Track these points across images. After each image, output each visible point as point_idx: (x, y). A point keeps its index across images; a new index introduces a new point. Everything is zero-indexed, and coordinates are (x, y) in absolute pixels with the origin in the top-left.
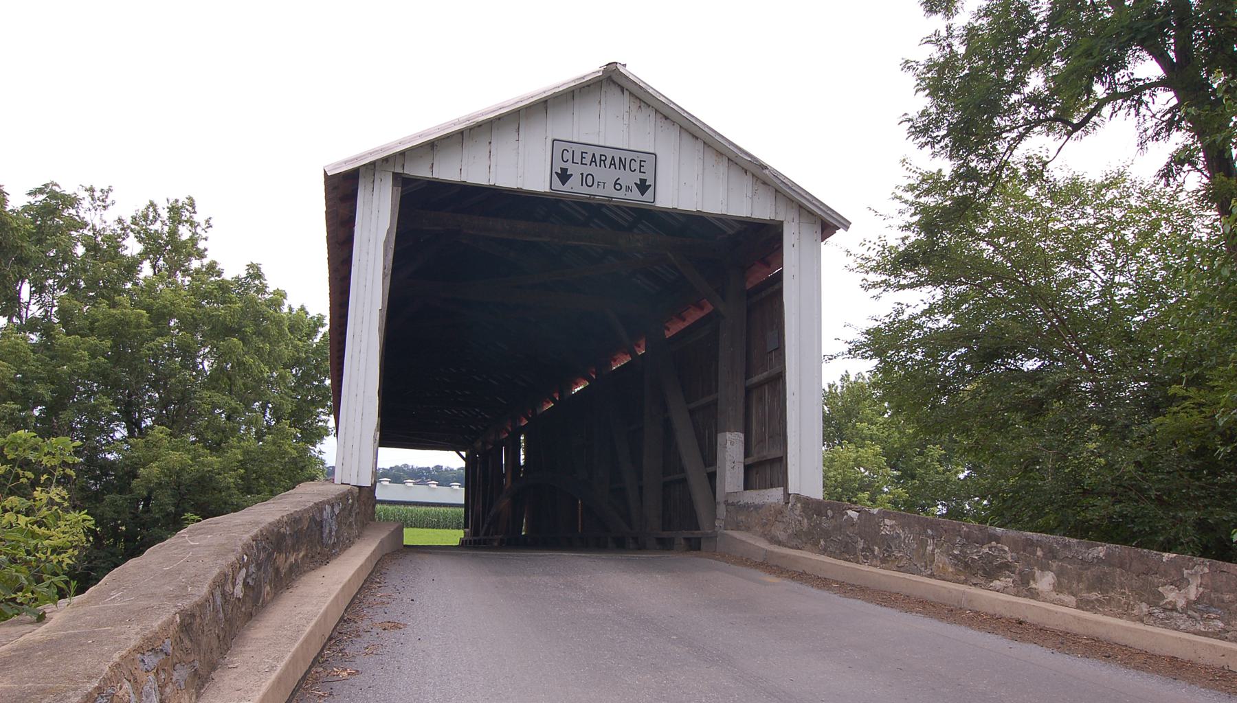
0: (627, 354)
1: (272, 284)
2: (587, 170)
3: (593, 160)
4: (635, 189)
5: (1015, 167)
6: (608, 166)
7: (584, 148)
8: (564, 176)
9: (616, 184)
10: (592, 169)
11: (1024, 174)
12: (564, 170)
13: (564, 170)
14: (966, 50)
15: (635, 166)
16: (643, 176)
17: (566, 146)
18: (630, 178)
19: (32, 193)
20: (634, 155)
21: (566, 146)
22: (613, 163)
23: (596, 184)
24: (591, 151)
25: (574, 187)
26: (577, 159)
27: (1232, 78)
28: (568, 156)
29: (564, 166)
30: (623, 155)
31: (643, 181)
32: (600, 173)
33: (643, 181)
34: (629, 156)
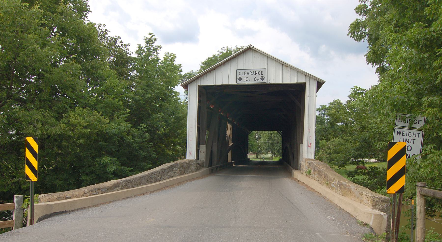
0: (255, 154)
1: (354, 17)
2: (246, 76)
3: (248, 73)
4: (260, 79)
5: (375, 119)
6: (252, 74)
7: (245, 71)
8: (240, 79)
9: (255, 79)
10: (248, 76)
11: (417, 167)
12: (240, 78)
13: (240, 78)
14: (374, 89)
15: (260, 73)
16: (262, 76)
17: (240, 71)
18: (258, 77)
19: (349, 30)
20: (259, 70)
21: (240, 71)
22: (253, 73)
23: (249, 80)
24: (247, 71)
25: (243, 82)
26: (243, 74)
27: (1, 16)
28: (241, 73)
29: (240, 76)
30: (256, 70)
31: (262, 77)
32: (250, 77)
33: (262, 77)
34: (258, 70)
